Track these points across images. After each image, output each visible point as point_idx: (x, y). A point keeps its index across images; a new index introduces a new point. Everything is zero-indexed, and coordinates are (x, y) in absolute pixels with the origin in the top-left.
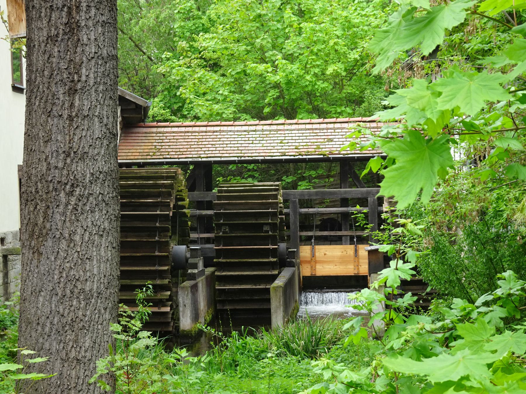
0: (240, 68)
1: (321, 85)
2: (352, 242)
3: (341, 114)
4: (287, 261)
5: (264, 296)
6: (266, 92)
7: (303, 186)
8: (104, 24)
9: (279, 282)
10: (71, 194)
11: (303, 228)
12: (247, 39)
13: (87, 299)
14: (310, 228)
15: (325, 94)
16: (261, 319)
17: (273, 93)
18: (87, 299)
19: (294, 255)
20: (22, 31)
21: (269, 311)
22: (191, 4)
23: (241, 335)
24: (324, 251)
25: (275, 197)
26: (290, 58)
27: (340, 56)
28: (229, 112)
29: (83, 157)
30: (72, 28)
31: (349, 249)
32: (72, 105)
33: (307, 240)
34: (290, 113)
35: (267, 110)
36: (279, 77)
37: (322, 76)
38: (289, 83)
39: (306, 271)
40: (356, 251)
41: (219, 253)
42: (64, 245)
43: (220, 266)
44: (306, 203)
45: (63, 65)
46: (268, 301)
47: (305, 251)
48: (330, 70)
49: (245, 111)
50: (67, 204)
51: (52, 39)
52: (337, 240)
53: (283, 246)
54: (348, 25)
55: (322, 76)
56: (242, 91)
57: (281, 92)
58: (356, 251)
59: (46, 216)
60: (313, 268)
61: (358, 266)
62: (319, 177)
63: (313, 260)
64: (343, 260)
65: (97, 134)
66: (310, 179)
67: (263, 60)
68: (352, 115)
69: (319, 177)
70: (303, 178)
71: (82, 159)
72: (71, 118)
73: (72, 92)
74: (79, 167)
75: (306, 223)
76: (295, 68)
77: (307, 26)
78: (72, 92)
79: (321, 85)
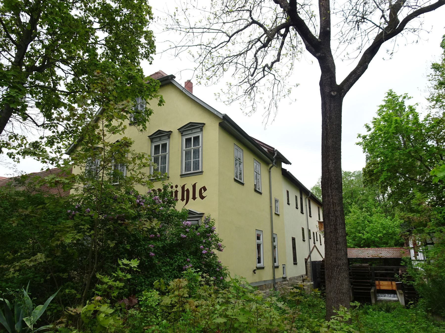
0: (354, 235)
1: (377, 239)
2: (390, 281)
3: (383, 247)
4: (373, 285)
5: (369, 294)
6: (361, 241)
7: (374, 266)
8: (343, 228)
9: (372, 291)
10: (337, 268)
11: (376, 276)
12: (356, 228)
13: (343, 294)
14: (377, 276)
15: (378, 242)
16: (369, 301)
17: (363, 241)
18: (343, 294)
19: (374, 283)
20: (323, 230)
21: (370, 298)
22: (4, 156)
23: (367, 304)
24: (382, 282)
25: (368, 268)
26: (367, 232)
27: (381, 232)
28: (352, 246)
29: (340, 259)
30: (336, 229)
31: (390, 283)
32: (337, 247)
33: (377, 280)
34: (369, 246)
35: (362, 245)
36: (365, 237)
37: (376, 237)
38: (368, 239)
39: (378, 288)
40: (392, 283)
41: (354, 282)
42: (337, 280)
43: (354, 285)
44: (375, 269)
45: (334, 238)
46: (370, 295)
47: (377, 282)
48: (379, 235)
49: (356, 245)
50: (337, 270)
51: (331, 232)
52: (386, 280)
53: (371, 281)
54: (382, 224)
55: (376, 237)
56: (354, 240)
57: (366, 241)
58: (392, 283)
59: (332, 273)
60: (379, 287)
61: (392, 287)
62: (378, 263)
63: (379, 285)
64: (388, 285)
65: (343, 254)
66: (375, 263)
67: (360, 233)
68: (385, 247)
69: (378, 263)
70: (373, 263)
71: (340, 260)
72: (336, 250)
73: (337, 244)
74: (339, 262)
75: (376, 275)
76: (369, 235)
77: (371, 225)
78: (337, 244)
79: (377, 239)
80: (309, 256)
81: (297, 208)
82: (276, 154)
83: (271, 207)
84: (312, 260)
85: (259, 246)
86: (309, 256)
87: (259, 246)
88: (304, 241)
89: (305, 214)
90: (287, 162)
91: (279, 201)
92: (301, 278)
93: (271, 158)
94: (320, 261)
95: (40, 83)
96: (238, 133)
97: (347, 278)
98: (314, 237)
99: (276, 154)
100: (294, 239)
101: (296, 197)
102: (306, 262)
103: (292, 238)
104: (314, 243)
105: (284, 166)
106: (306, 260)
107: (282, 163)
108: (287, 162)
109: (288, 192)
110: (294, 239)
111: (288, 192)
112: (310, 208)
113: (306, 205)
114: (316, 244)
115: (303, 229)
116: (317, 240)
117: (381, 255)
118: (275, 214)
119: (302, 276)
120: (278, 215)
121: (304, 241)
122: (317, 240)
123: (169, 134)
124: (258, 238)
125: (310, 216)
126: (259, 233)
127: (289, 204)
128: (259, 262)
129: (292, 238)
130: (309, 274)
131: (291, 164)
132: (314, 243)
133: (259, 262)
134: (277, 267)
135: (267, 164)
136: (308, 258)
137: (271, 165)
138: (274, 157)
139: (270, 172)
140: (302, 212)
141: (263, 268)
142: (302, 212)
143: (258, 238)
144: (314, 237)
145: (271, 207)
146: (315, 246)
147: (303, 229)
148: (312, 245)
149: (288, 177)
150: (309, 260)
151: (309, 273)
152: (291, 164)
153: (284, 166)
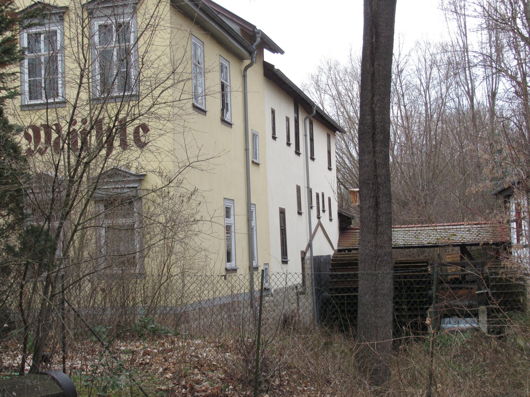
29: (381, 247)
74: (380, 251)
80: (310, 246)
81: (289, 144)
82: (258, 40)
83: (247, 150)
84: (315, 254)
85: (228, 228)
86: (310, 246)
87: (228, 228)
88: (300, 213)
89: (303, 156)
90: (275, 49)
91: (260, 135)
92: (295, 291)
93: (245, 42)
94: (329, 256)
95: (35, 30)
96: (217, 27)
97: (379, 288)
98: (318, 203)
99: (258, 40)
100: (282, 212)
101: (288, 119)
102: (303, 259)
103: (280, 208)
104: (319, 218)
105: (269, 56)
106: (304, 254)
107: (265, 50)
108: (275, 49)
109: (273, 112)
110: (282, 212)
111: (273, 112)
112: (312, 140)
113: (306, 135)
114: (322, 220)
115: (298, 189)
116: (324, 211)
117: (454, 237)
118: (253, 162)
119: (296, 287)
120: (258, 164)
121: (300, 213)
122: (324, 211)
123: (61, 13)
124: (228, 215)
125: (313, 159)
126: (228, 204)
127: (274, 138)
128: (229, 260)
129: (280, 208)
130: (308, 283)
131: (282, 52)
132: (319, 218)
133: (229, 260)
134: (257, 268)
135: (240, 58)
136: (307, 249)
137: (247, 62)
138: (254, 46)
139: (244, 77)
140: (298, 153)
141: (235, 270)
142: (298, 153)
143: (228, 215)
144: (318, 203)
145: (247, 150)
146: (320, 224)
147: (298, 189)
148: (315, 221)
149: (275, 78)
150: (308, 255)
151: (308, 283)
152: (282, 52)
153: (269, 56)
